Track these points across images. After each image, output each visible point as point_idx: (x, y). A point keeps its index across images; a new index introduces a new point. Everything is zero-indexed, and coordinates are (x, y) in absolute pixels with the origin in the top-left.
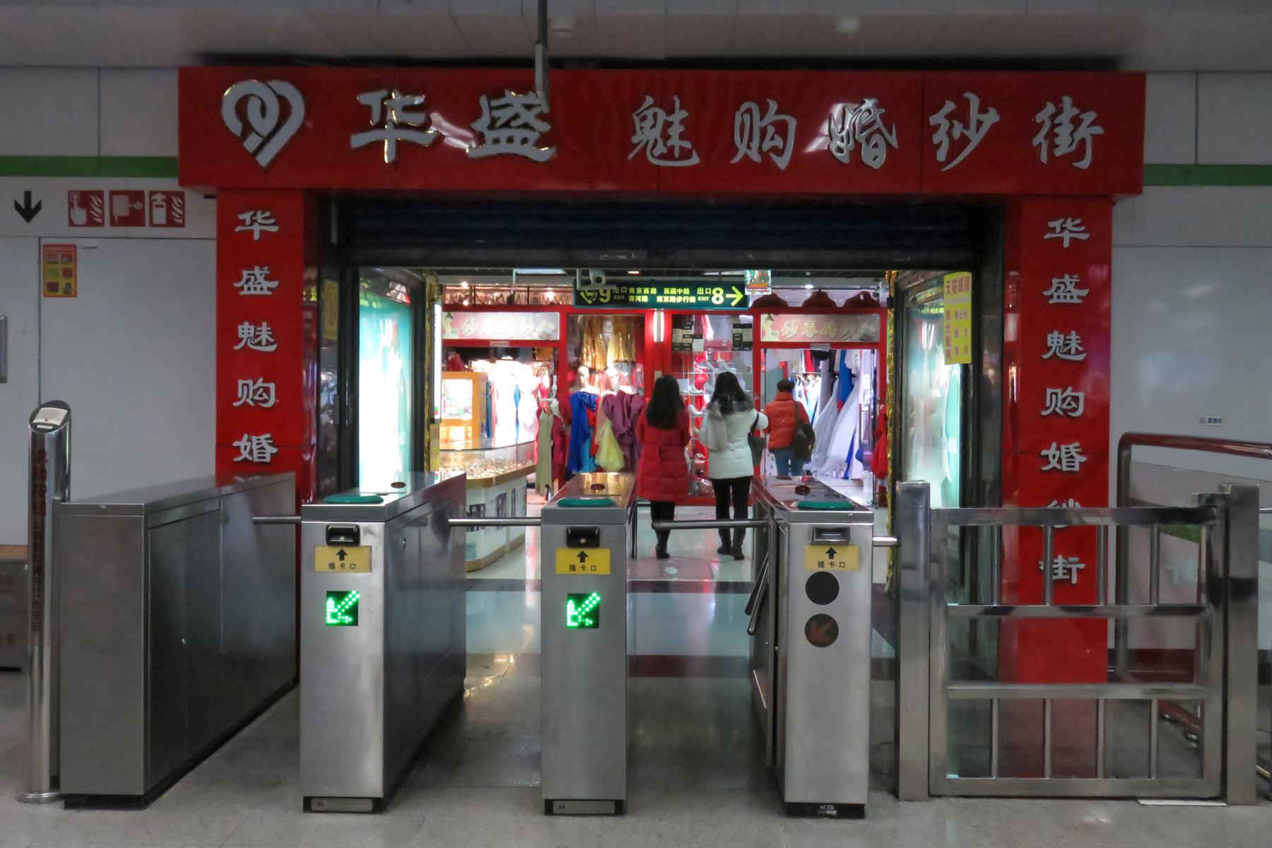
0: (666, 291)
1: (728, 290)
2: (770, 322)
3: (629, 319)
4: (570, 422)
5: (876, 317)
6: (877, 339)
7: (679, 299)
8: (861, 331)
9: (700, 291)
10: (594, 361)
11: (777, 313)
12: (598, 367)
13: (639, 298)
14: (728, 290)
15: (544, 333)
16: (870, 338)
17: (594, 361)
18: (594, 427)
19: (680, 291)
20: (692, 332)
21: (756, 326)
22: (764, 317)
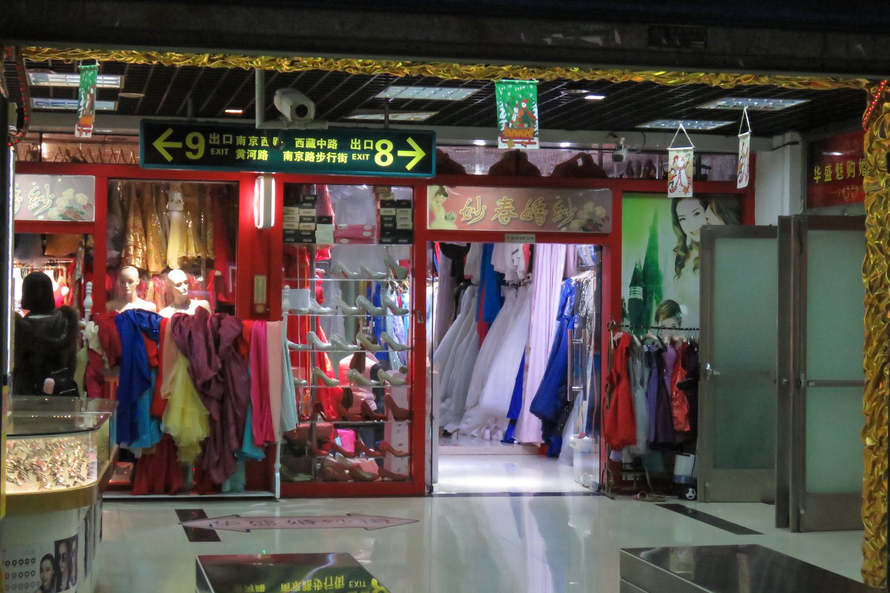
0: (299, 142)
1: (400, 143)
2: (442, 198)
3: (202, 188)
4: (118, 361)
5: (605, 192)
6: (607, 228)
7: (321, 157)
8: (584, 216)
9: (355, 144)
10: (146, 259)
11: (452, 184)
12: (154, 268)
13: (252, 154)
14: (400, 143)
15: (70, 209)
16: (597, 226)
17: (146, 259)
18: (158, 369)
19: (322, 143)
20: (313, 212)
21: (418, 206)
22: (432, 190)
